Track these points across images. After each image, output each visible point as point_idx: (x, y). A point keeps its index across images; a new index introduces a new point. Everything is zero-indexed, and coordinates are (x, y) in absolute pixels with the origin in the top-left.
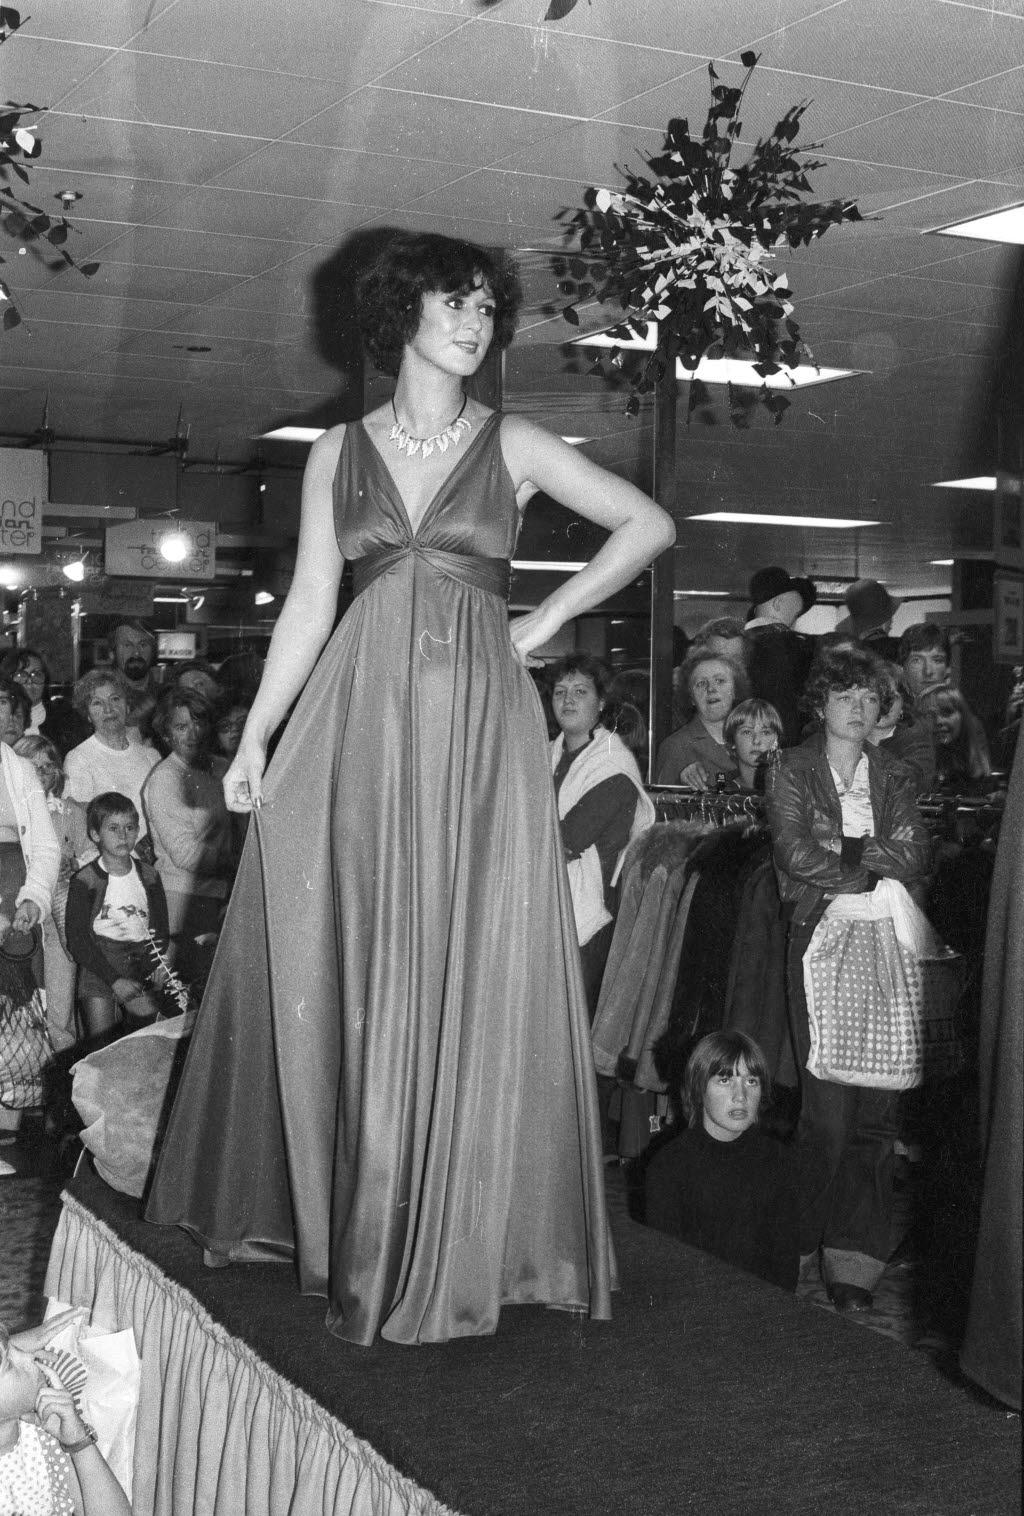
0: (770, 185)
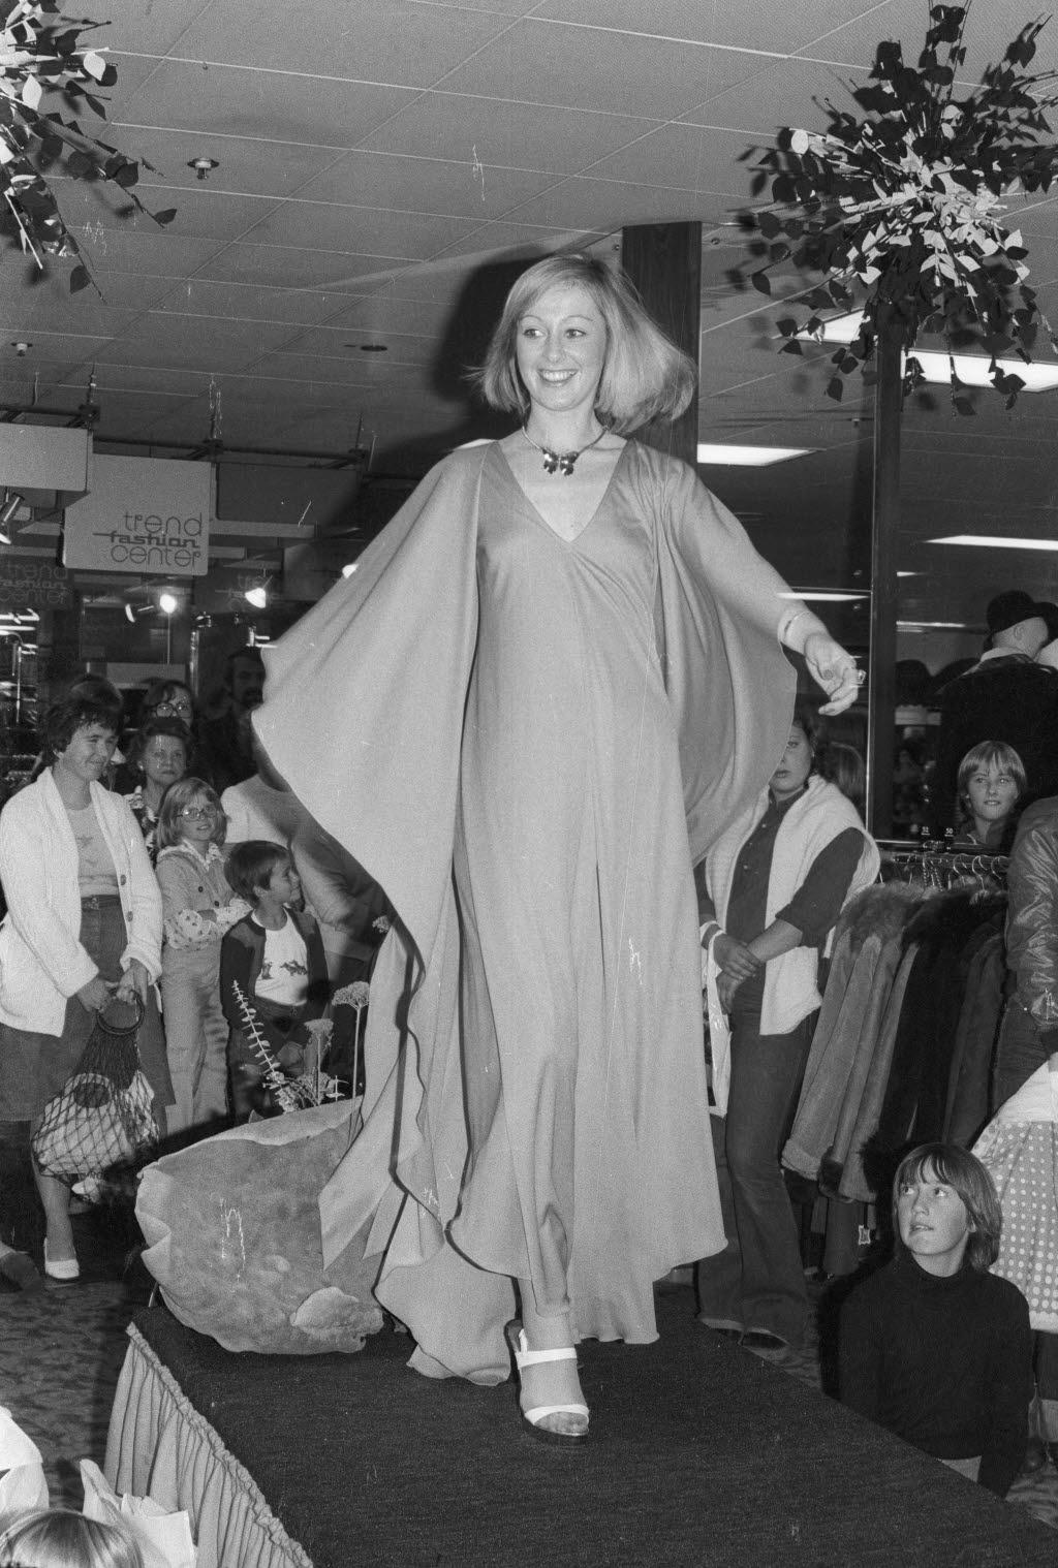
0: (1001, 124)
